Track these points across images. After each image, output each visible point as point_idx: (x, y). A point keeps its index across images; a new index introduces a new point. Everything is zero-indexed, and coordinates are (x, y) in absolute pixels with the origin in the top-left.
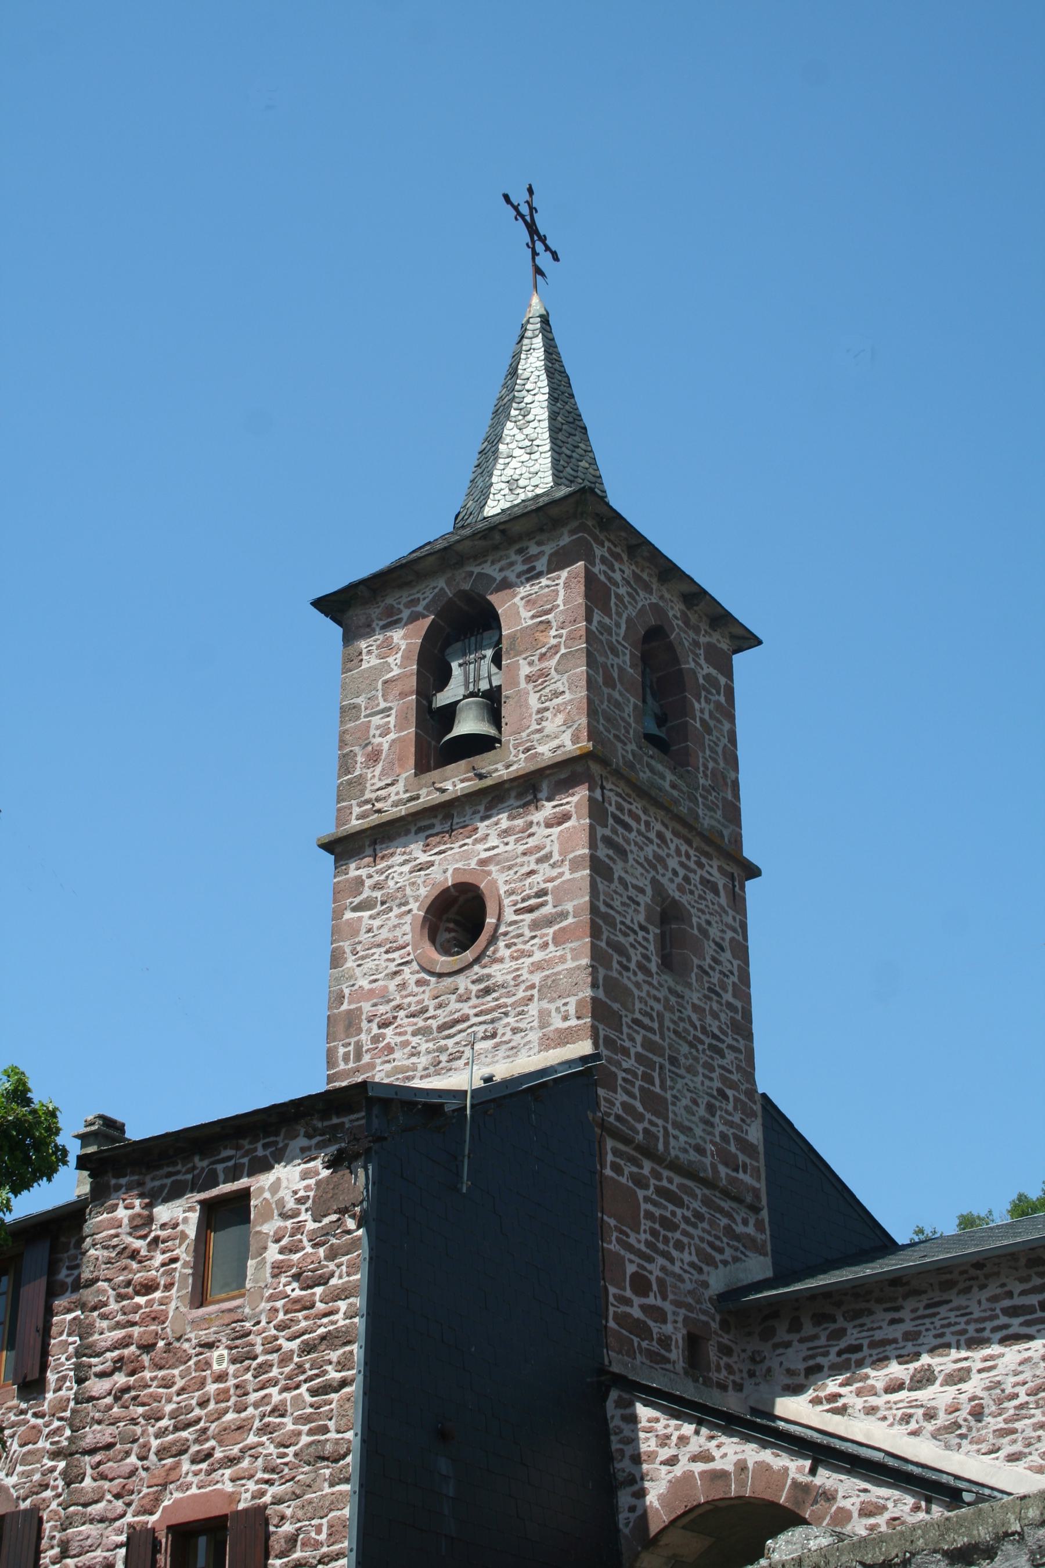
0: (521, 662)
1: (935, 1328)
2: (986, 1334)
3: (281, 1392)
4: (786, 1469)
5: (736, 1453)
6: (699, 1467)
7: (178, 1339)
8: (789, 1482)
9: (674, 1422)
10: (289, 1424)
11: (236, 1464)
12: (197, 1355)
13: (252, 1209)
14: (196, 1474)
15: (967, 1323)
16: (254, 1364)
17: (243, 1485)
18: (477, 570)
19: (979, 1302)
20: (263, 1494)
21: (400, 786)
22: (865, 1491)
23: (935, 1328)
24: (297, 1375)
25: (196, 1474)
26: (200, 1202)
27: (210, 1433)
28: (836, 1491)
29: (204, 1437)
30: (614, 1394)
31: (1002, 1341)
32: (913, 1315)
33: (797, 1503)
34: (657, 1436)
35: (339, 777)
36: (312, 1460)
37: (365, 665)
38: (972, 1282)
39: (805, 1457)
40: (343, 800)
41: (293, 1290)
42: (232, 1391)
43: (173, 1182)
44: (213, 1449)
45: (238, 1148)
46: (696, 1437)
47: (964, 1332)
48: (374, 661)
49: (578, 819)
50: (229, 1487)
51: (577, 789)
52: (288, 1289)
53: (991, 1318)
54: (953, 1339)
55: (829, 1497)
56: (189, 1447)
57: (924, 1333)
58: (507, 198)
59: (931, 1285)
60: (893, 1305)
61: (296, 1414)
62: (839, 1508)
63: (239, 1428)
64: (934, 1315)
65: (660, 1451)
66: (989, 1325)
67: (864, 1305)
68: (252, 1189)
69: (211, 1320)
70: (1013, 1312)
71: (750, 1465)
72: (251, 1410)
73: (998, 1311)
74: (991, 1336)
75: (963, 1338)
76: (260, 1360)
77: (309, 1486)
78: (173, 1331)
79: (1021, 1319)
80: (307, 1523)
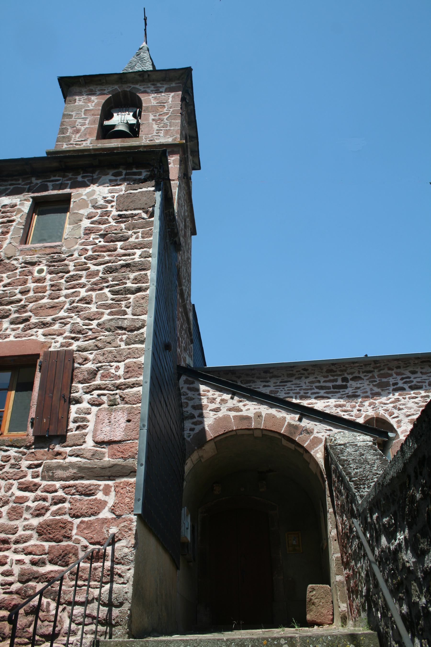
0: (150, 114)
1: (285, 390)
2: (309, 395)
3: (87, 291)
4: (285, 418)
5: (255, 409)
6: (232, 414)
7: (9, 258)
8: (286, 424)
9: (218, 393)
10: (93, 308)
11: (48, 327)
12: (22, 268)
13: (72, 203)
14: (13, 330)
15: (300, 390)
16: (67, 275)
17: (54, 339)
18: (132, 86)
19: (305, 383)
20: (70, 344)
21: (89, 142)
22: (330, 430)
23: (285, 390)
24: (101, 283)
25: (13, 330)
26: (32, 198)
27: (29, 308)
28: (313, 429)
29: (23, 310)
30: (183, 378)
31: (316, 398)
32: (275, 385)
33: (291, 433)
34: (208, 398)
35: (59, 134)
36: (112, 328)
37: (76, 104)
38: (302, 375)
39: (296, 413)
40: (59, 142)
41: (100, 242)
42: (48, 288)
43: (14, 188)
44: (30, 317)
45: (64, 176)
46: (231, 400)
47: (298, 393)
48: (81, 103)
49: (174, 165)
50: (42, 339)
51: (174, 156)
52: (97, 241)
53: (311, 389)
54: (294, 395)
55: (309, 432)
56: (10, 314)
57: (280, 392)
58: (144, 9)
59: (283, 374)
60: (265, 380)
61: (99, 303)
62: (315, 437)
63: (52, 307)
64: (285, 385)
65: (210, 405)
66: (310, 392)
67: (251, 379)
68: (72, 194)
69: (36, 251)
70: (321, 388)
71: (264, 415)
72: (62, 299)
73: (314, 387)
74: (311, 396)
75: (298, 396)
76: (71, 273)
77: (109, 343)
78: (5, 254)
79: (325, 391)
80: (107, 364)
